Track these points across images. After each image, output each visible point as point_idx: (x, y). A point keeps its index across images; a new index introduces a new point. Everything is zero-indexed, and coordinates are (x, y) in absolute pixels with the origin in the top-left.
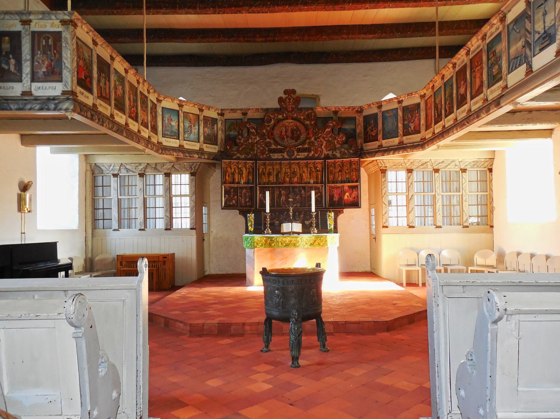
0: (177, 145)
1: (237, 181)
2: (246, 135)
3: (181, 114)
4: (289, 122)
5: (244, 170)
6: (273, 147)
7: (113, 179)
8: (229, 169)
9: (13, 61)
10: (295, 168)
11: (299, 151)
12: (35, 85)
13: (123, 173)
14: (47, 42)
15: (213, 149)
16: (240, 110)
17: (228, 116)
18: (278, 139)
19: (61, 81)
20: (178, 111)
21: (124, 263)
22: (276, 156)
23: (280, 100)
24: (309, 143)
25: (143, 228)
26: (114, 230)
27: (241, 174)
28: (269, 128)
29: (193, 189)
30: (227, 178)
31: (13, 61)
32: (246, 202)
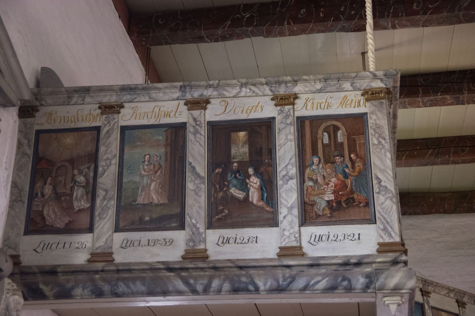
9: (255, 182)
31: (255, 182)
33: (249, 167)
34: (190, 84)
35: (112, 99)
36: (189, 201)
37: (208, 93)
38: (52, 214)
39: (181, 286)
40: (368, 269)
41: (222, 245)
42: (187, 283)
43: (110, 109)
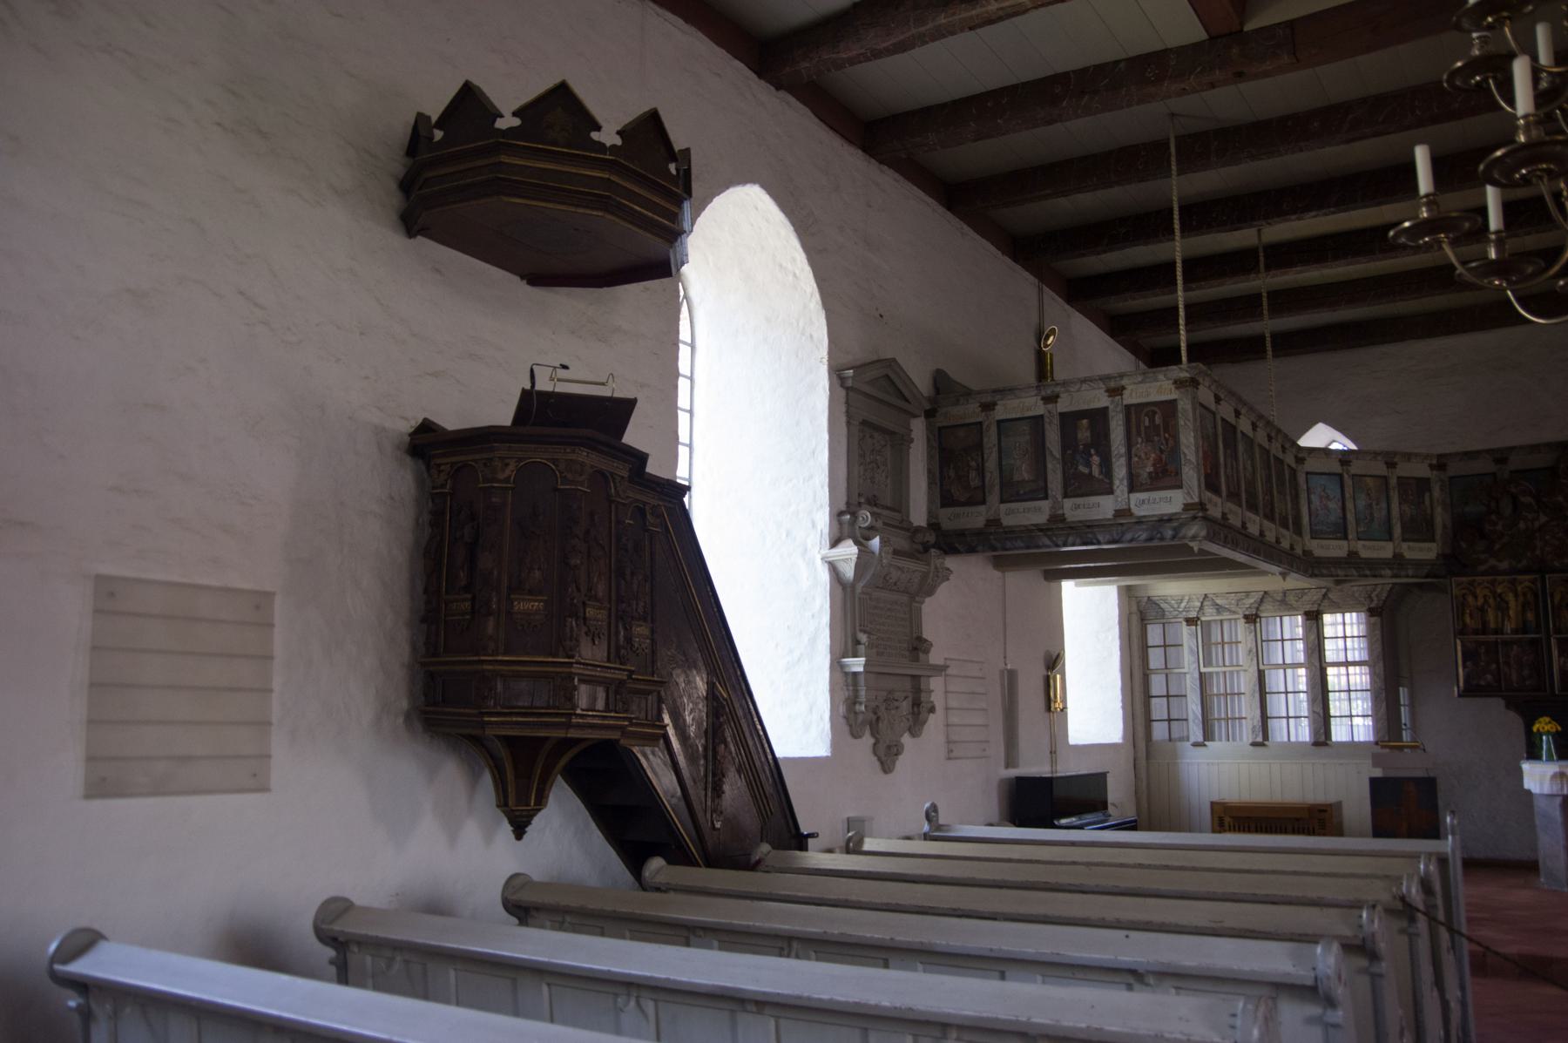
0: (1343, 553)
1: (1492, 625)
3: (1348, 481)
7: (1186, 630)
8: (1470, 599)
9: (1096, 459)
12: (1136, 497)
13: (1209, 615)
14: (1152, 420)
15: (1427, 552)
16: (1488, 451)
17: (1454, 469)
19: (1180, 487)
20: (1341, 476)
21: (1227, 820)
25: (1260, 739)
26: (1196, 745)
27: (1502, 607)
29: (1378, 647)
30: (1468, 620)
31: (1096, 459)
34: (1411, 930)
35: (988, 399)
36: (1050, 477)
37: (1058, 389)
39: (1048, 542)
40: (1175, 524)
41: (1078, 510)
42: (1050, 538)
43: (988, 407)
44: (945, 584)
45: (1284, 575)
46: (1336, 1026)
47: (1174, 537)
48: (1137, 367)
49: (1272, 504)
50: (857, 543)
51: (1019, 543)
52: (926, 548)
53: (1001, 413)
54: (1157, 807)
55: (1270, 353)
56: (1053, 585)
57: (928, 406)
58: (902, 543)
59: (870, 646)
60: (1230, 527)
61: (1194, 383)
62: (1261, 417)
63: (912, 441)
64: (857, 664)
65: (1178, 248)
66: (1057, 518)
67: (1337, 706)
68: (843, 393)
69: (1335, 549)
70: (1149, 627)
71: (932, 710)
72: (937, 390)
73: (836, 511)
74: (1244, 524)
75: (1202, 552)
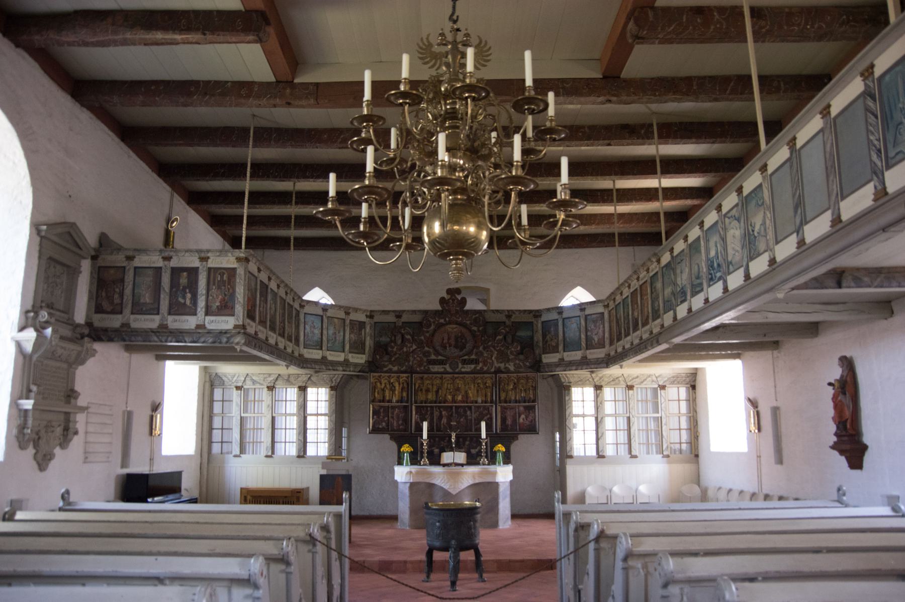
1: (387, 398)
2: (399, 342)
4: (452, 329)
5: (397, 385)
6: (433, 357)
7: (235, 393)
8: (378, 384)
9: (189, 295)
10: (460, 383)
11: (465, 362)
12: (208, 318)
14: (222, 277)
16: (393, 311)
17: (378, 318)
18: (438, 348)
19: (233, 315)
21: (249, 498)
22: (436, 368)
23: (442, 301)
24: (476, 354)
25: (270, 454)
26: (235, 456)
27: (393, 390)
28: (428, 335)
29: (334, 406)
31: (189, 295)
32: (399, 425)
33: (334, 172)
35: (130, 253)
36: (162, 302)
37: (172, 254)
38: (106, 305)
39: (156, 339)
42: (158, 337)
43: (130, 258)
44: (92, 359)
45: (287, 367)
46: (258, 598)
47: (227, 342)
48: (224, 246)
49: (284, 328)
50: (36, 330)
51: (140, 338)
52: (82, 336)
53: (137, 262)
54: (211, 491)
55: (292, 248)
56: (161, 363)
57: (93, 253)
58: (66, 332)
59: (38, 393)
60: (259, 339)
61: (247, 260)
62: (283, 282)
63: (81, 272)
64: (28, 404)
65: (247, 185)
66: (163, 326)
67: (310, 436)
68: (38, 239)
69: (316, 354)
70: (216, 390)
71: (76, 433)
72: (101, 245)
73: (24, 310)
74: (267, 338)
75: (241, 351)
